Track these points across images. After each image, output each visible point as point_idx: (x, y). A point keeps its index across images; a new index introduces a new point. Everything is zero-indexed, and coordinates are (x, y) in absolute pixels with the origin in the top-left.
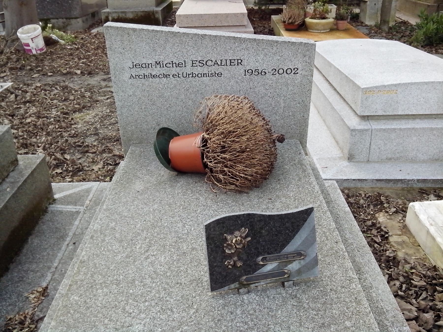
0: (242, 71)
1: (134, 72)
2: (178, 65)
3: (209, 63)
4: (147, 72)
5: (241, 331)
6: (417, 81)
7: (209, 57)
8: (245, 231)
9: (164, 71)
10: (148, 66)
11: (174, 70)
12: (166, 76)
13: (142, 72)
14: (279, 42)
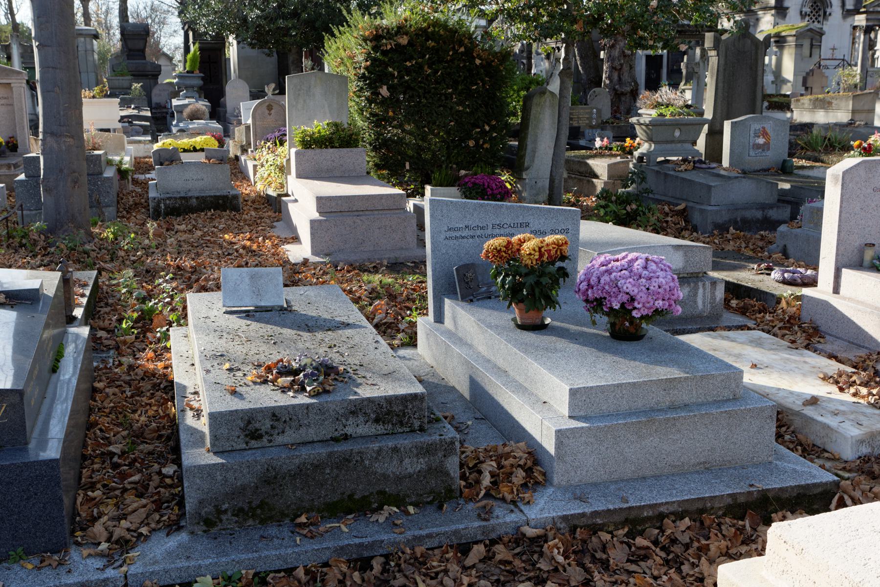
0: (531, 225)
1: (449, 234)
2: (482, 228)
3: (505, 226)
4: (458, 234)
5: (549, 4)
6: (551, 156)
7: (505, 221)
8: (447, 302)
9: (471, 233)
10: (459, 229)
11: (479, 232)
12: (472, 237)
13: (454, 234)
14: (831, 380)
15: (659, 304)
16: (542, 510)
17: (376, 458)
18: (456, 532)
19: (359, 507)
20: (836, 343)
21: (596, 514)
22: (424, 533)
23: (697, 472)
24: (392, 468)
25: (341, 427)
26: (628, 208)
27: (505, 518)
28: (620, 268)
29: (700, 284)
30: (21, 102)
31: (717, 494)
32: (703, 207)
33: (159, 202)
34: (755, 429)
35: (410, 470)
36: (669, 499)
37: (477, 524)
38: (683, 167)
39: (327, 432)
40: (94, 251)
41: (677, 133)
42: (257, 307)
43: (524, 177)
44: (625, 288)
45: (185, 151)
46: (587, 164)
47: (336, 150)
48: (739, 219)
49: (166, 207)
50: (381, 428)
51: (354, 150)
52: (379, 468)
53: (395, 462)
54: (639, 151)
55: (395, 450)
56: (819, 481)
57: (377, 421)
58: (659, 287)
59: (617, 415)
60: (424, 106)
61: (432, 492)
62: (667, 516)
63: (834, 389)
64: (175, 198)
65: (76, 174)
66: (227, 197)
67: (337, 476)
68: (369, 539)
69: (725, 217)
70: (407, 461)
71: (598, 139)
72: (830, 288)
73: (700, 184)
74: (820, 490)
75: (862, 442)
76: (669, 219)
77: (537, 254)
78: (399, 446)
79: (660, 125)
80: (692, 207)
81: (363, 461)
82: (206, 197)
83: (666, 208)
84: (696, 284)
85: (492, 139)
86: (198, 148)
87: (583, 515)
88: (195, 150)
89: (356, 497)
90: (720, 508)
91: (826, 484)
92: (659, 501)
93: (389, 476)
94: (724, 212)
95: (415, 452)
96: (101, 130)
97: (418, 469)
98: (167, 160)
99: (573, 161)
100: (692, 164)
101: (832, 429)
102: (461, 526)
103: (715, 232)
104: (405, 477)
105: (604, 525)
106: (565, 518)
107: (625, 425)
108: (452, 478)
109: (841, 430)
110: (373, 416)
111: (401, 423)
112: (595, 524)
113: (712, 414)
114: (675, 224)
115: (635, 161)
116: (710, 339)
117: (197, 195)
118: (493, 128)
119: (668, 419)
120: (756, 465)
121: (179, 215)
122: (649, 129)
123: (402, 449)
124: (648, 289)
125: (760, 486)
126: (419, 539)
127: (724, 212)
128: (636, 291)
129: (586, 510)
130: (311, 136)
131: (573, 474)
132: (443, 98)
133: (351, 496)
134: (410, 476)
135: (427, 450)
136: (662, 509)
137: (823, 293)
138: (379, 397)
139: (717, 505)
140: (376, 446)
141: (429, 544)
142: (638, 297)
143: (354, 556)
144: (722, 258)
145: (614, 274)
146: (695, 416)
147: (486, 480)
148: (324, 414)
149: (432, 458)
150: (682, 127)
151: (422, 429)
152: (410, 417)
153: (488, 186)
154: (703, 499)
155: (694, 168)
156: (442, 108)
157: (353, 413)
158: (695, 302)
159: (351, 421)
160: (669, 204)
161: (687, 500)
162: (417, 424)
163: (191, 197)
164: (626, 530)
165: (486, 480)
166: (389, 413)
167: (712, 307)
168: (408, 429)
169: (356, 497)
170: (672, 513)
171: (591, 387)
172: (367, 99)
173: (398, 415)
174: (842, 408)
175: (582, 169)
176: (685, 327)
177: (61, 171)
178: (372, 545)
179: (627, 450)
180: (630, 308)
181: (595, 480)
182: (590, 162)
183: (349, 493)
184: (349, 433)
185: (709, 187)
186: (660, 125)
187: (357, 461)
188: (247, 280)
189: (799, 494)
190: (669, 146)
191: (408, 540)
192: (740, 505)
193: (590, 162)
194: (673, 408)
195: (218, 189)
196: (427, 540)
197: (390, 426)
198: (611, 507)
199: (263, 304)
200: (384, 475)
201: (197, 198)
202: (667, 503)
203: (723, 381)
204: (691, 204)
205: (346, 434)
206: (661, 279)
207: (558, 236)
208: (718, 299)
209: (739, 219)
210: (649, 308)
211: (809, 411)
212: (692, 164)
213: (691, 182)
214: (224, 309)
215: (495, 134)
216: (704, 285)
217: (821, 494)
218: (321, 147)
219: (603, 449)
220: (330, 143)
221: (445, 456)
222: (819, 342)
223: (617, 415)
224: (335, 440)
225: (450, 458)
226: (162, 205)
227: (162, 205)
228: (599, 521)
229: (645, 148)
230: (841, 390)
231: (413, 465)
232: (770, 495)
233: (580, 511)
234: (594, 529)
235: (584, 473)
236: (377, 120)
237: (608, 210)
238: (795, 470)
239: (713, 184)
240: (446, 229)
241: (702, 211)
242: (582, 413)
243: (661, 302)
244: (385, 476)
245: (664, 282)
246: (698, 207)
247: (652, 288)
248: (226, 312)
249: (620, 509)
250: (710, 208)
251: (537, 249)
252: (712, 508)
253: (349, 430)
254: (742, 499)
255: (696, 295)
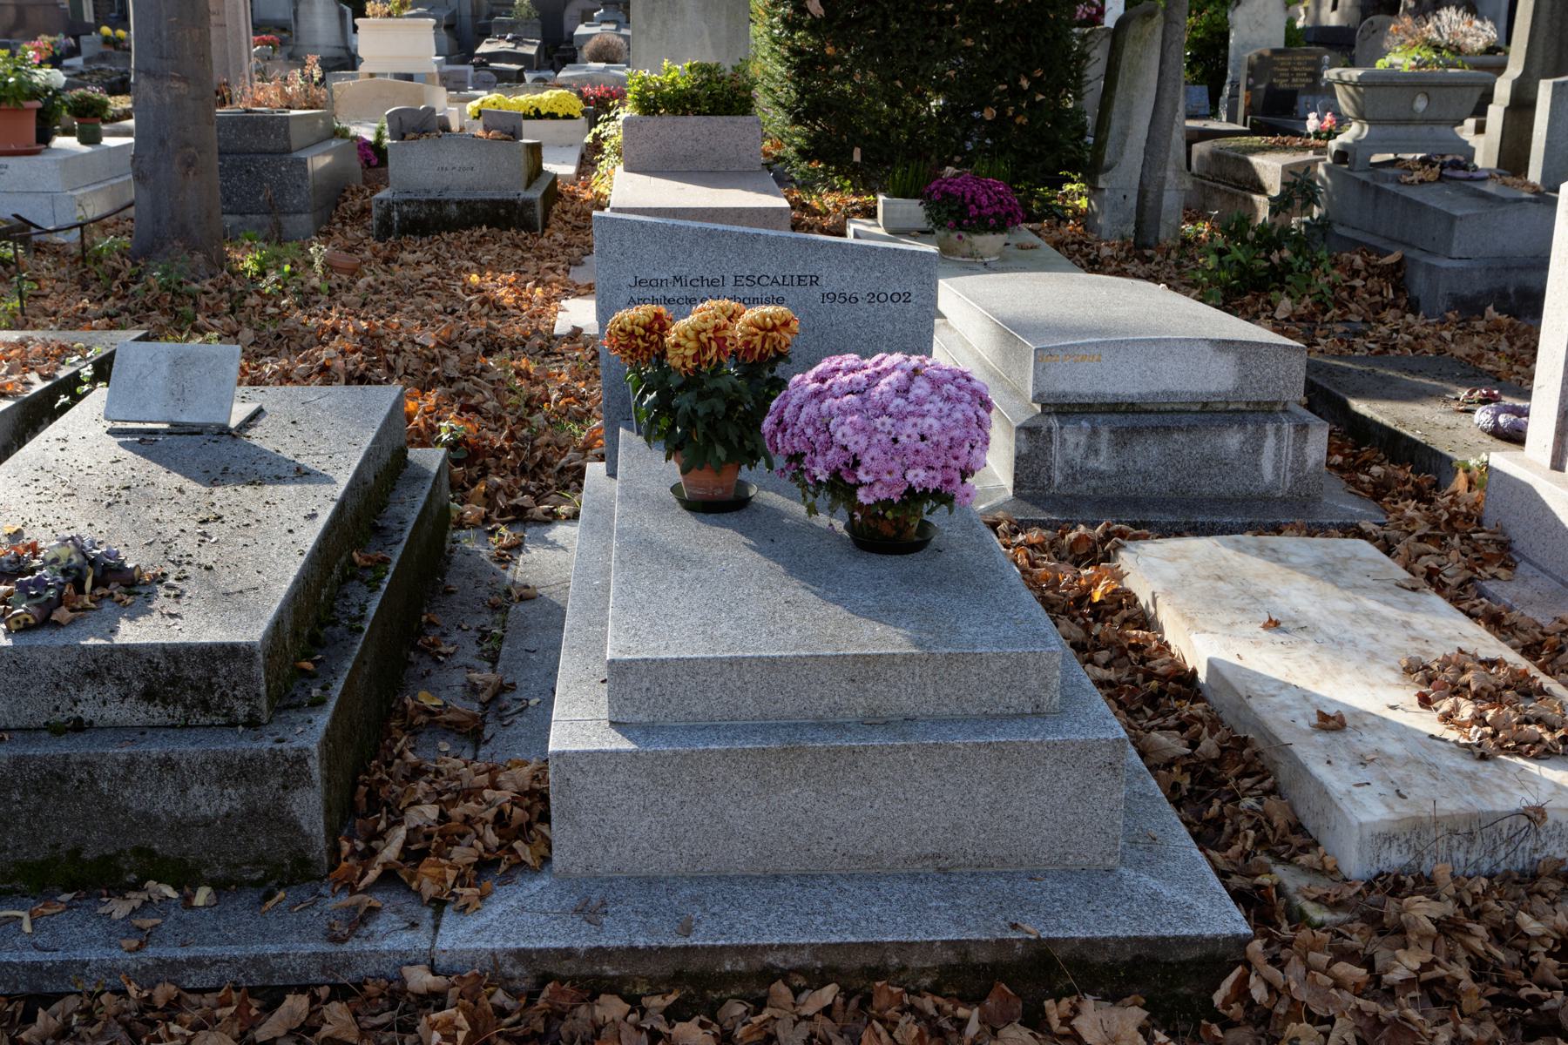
3: (764, 281)
7: (764, 270)
10: (660, 283)
15: (917, 476)
16: (502, 925)
17: (124, 779)
18: (258, 961)
19: (91, 878)
20: (1534, 583)
21: (600, 954)
22: (181, 954)
23: (914, 877)
24: (163, 801)
25: (68, 703)
26: (1275, 257)
27: (392, 939)
28: (847, 389)
29: (1270, 428)
30: (237, 21)
31: (920, 936)
32: (1434, 261)
33: (389, 208)
34: (1070, 790)
35: (205, 810)
36: (793, 939)
37: (310, 947)
38: (1417, 176)
39: (36, 710)
40: (206, 293)
41: (1421, 104)
42: (173, 424)
43: (1101, 185)
44: (839, 435)
45: (527, 117)
46: (1249, 164)
47: (703, 119)
48: (1511, 290)
49: (403, 217)
50: (158, 714)
51: (740, 119)
52: (134, 798)
53: (169, 791)
54: (1340, 139)
55: (167, 764)
56: (1194, 932)
57: (148, 695)
58: (923, 438)
59: (712, 728)
60: (895, 36)
61: (258, 862)
62: (785, 975)
63: (1407, 696)
64: (420, 202)
65: (193, 150)
66: (513, 203)
67: (39, 809)
68: (58, 957)
69: (1480, 283)
70: (196, 789)
71: (1312, 116)
72: (1546, 459)
73: (1436, 211)
74: (1196, 953)
75: (1388, 838)
76: (1358, 282)
77: (691, 344)
78: (175, 757)
79: (1382, 85)
80: (1414, 261)
81: (94, 781)
82: (476, 202)
83: (1358, 260)
84: (1260, 426)
85: (1033, 105)
86: (543, 112)
87: (568, 953)
88: (538, 115)
89: (86, 856)
90: (923, 971)
91: (1214, 940)
92: (765, 941)
93: (158, 819)
94: (1476, 274)
95: (214, 772)
96: (398, 76)
97: (225, 808)
98: (414, 130)
99: (1227, 157)
100: (1437, 168)
101: (1331, 800)
102: (273, 949)
103: (1451, 315)
104: (195, 824)
105: (622, 980)
106: (522, 956)
107: (726, 754)
108: (306, 837)
109: (1346, 805)
110: (139, 685)
111: (207, 708)
112: (599, 978)
113: (953, 747)
114: (1371, 294)
115: (1329, 160)
116: (1229, 553)
117: (458, 196)
118: (1036, 84)
119: (838, 751)
120: (1068, 874)
121: (424, 234)
122: (1358, 92)
123: (183, 764)
124: (895, 441)
125: (1035, 928)
126: (170, 968)
127: (1476, 274)
128: (863, 443)
129: (577, 944)
130: (656, 90)
131: (599, 852)
132: (934, 21)
133: (76, 852)
134: (207, 823)
135: (243, 771)
136: (769, 959)
137: (1528, 465)
138: (148, 646)
139: (915, 963)
140: (122, 752)
141: (194, 981)
142: (866, 459)
143: (23, 988)
144: (1412, 372)
145: (829, 401)
146: (909, 748)
147: (390, 851)
148: (27, 672)
149: (255, 789)
150: (1432, 91)
151: (253, 723)
152: (223, 694)
153: (973, 200)
154: (878, 946)
155: (1441, 178)
156: (932, 42)
157: (92, 675)
158: (1257, 467)
159: (88, 692)
160: (1367, 249)
161: (837, 945)
162: (242, 710)
163: (447, 202)
164: (671, 998)
165: (390, 851)
166: (173, 681)
167: (1297, 480)
168: (222, 720)
169: (86, 856)
170: (799, 971)
171: (664, 662)
172: (784, 20)
173: (197, 689)
174: (1393, 748)
175: (1240, 175)
176: (1215, 519)
177: (162, 142)
178: (63, 968)
179: (732, 810)
180: (851, 481)
181: (654, 869)
182: (1255, 160)
183: (68, 845)
184: (86, 718)
185: (1451, 219)
186: (1382, 85)
187: (81, 781)
188: (164, 369)
189: (1139, 957)
190: (1401, 131)
191: (145, 967)
192: (977, 969)
193: (1255, 160)
194: (874, 722)
195: (500, 188)
196: (190, 971)
197: (180, 709)
198: (640, 942)
199: (184, 419)
200: (145, 815)
201: (459, 203)
202: (782, 947)
203: (1006, 670)
204: (1414, 254)
205: (80, 719)
206: (929, 421)
207: (770, 309)
208: (1311, 463)
209: (1511, 290)
210: (890, 486)
211: (1311, 753)
212: (1437, 168)
213: (1420, 206)
214: (109, 425)
215: (1040, 97)
216: (1278, 429)
217: (1200, 962)
218: (675, 113)
219: (673, 804)
220: (694, 105)
221: (285, 787)
222: (1494, 576)
223: (712, 728)
224: (56, 730)
225: (297, 793)
226: (395, 214)
227: (395, 214)
228: (609, 970)
229: (1352, 133)
230: (1425, 701)
231: (211, 801)
232: (1059, 954)
233: (562, 944)
234: (593, 988)
235: (627, 853)
236: (802, 62)
237: (1228, 258)
238: (1155, 897)
239: (1458, 213)
240: (631, 281)
241: (1430, 269)
242: (642, 717)
243: (922, 474)
244: (148, 819)
245: (936, 425)
246: (1426, 259)
247: (903, 439)
248: (112, 432)
249: (663, 949)
250: (1445, 263)
251: (691, 334)
252: (904, 969)
253: (87, 711)
254: (984, 957)
255: (1257, 451)
